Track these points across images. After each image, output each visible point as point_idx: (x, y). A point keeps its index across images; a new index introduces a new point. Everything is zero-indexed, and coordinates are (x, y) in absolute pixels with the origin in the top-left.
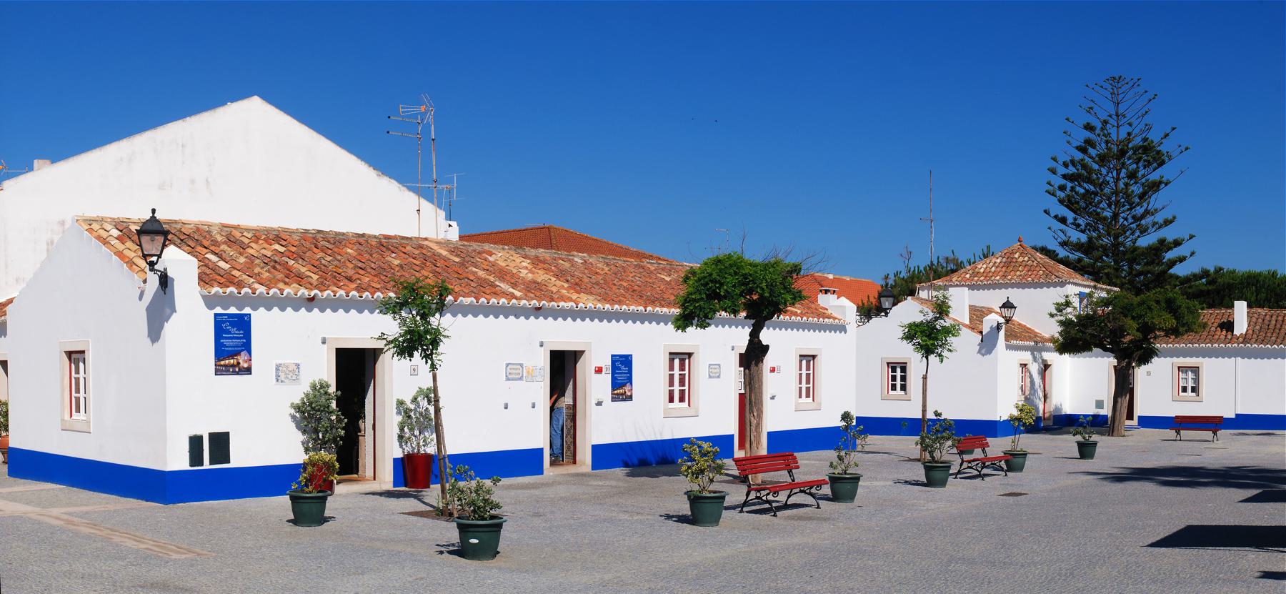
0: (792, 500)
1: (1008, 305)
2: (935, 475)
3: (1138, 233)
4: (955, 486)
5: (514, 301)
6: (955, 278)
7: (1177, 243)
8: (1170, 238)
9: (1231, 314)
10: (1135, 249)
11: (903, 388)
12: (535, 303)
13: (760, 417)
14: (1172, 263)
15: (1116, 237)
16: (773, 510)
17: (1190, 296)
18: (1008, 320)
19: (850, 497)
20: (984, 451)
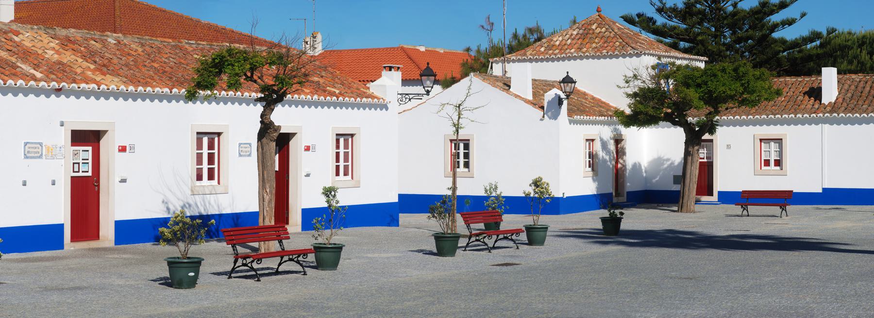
0: (498, 244)
1: (568, 80)
2: (445, 245)
5: (32, 83)
6: (529, 52)
11: (467, 165)
12: (54, 84)
14: (774, 27)
19: (334, 264)
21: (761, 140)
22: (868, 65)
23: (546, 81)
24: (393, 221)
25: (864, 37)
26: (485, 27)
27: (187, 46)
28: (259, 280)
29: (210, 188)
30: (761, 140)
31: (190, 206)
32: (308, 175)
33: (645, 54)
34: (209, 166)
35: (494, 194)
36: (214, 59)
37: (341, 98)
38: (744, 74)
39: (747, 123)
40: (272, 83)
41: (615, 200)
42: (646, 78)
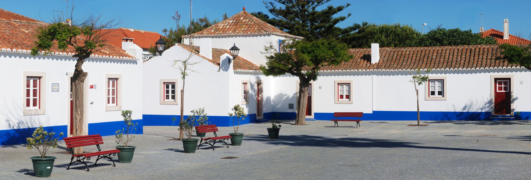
0: (99, 162)
1: (235, 48)
2: (189, 146)
3: (316, 4)
4: (199, 152)
6: (205, 32)
7: (340, 9)
8: (335, 6)
9: (370, 51)
10: (314, 13)
11: (173, 97)
13: (82, 114)
14: (337, 21)
15: (303, 6)
16: (86, 167)
17: (345, 40)
18: (235, 57)
19: (129, 159)
20: (215, 133)
21: (338, 84)
22: (386, 43)
23: (216, 49)
24: (140, 131)
25: (383, 27)
26: (175, 17)
27: (15, 23)
28: (88, 170)
29: (35, 111)
30: (338, 84)
31: (23, 123)
32: (92, 103)
33: (272, 34)
34: (33, 97)
35: (202, 115)
36: (50, 30)
37: (111, 56)
38: (335, 46)
39: (331, 74)
40: (83, 45)
41: (258, 118)
42: (276, 49)
